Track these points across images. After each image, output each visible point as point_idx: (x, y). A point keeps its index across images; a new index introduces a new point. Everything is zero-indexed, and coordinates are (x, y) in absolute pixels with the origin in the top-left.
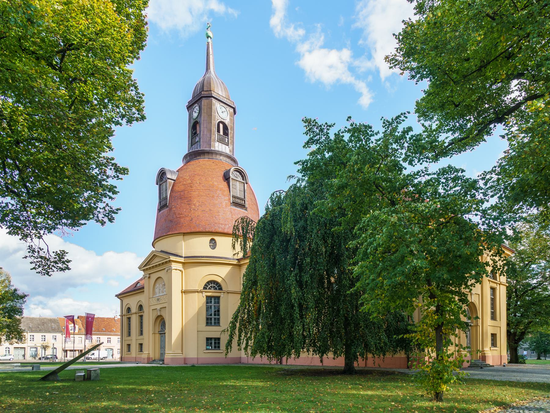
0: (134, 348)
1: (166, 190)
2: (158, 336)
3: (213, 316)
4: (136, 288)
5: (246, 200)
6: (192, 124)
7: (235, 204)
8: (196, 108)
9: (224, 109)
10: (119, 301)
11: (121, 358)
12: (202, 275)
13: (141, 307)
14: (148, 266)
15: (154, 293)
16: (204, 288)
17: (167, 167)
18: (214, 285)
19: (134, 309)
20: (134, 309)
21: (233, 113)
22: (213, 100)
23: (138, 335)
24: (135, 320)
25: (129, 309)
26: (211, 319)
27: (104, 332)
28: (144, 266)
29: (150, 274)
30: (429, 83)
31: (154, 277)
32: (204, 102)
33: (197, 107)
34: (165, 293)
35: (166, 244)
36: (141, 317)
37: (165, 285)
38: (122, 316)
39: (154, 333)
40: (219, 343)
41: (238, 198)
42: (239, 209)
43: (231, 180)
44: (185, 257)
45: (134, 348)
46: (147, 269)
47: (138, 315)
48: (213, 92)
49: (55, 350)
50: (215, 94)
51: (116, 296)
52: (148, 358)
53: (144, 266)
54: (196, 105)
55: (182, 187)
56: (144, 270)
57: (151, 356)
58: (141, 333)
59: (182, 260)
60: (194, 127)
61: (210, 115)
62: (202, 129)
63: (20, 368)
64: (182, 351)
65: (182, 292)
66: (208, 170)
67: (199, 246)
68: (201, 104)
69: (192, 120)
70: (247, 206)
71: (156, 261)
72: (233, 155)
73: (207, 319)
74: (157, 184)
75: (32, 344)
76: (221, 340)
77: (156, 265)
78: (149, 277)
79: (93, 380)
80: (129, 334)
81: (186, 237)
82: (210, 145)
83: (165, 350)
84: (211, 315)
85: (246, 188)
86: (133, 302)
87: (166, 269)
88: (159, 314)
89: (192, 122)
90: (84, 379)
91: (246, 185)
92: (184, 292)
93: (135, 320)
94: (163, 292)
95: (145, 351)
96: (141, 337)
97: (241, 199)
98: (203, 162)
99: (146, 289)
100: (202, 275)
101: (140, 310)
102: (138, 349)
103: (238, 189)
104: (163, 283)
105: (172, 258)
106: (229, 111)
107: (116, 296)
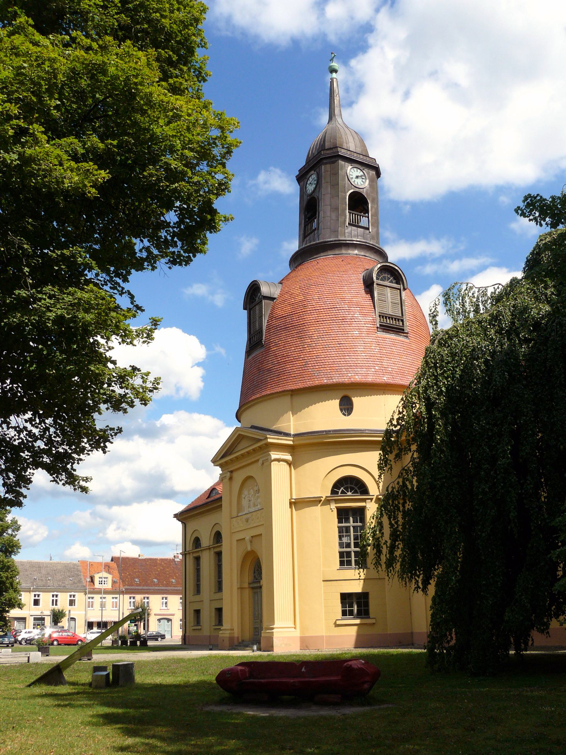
0: (207, 616)
2: (247, 592)
3: (353, 549)
4: (210, 500)
5: (406, 318)
6: (305, 203)
7: (385, 328)
8: (313, 178)
9: (359, 173)
10: (179, 525)
11: (184, 638)
12: (322, 473)
13: (218, 537)
14: (226, 457)
16: (333, 492)
17: (259, 277)
19: (206, 541)
20: (206, 541)
22: (341, 162)
23: (213, 590)
25: (197, 542)
26: (349, 554)
27: (155, 585)
28: (223, 457)
29: (231, 472)
30: (377, 506)
31: (239, 477)
32: (325, 168)
33: (314, 176)
34: (259, 507)
35: (258, 415)
36: (219, 554)
38: (185, 554)
39: (241, 588)
40: (367, 604)
41: (391, 317)
42: (393, 336)
43: (375, 285)
44: (295, 435)
45: (207, 616)
46: (226, 462)
47: (212, 552)
48: (339, 149)
49: (72, 623)
50: (343, 151)
51: (176, 516)
53: (223, 457)
54: (313, 172)
56: (221, 466)
61: (335, 185)
62: (325, 210)
63: (11, 659)
64: (295, 623)
65: (291, 503)
66: (339, 281)
69: (305, 197)
70: (407, 329)
71: (244, 448)
73: (341, 554)
74: (245, 309)
77: (242, 456)
78: (231, 478)
80: (198, 590)
81: (298, 400)
82: (336, 232)
83: (261, 622)
84: (348, 545)
85: (403, 298)
86: (204, 528)
87: (260, 461)
88: (249, 549)
89: (306, 198)
91: (403, 293)
92: (297, 504)
94: (255, 505)
96: (218, 596)
98: (324, 262)
99: (225, 503)
100: (322, 473)
102: (213, 619)
103: (390, 300)
104: (256, 488)
105: (272, 439)
106: (368, 174)
107: (176, 516)
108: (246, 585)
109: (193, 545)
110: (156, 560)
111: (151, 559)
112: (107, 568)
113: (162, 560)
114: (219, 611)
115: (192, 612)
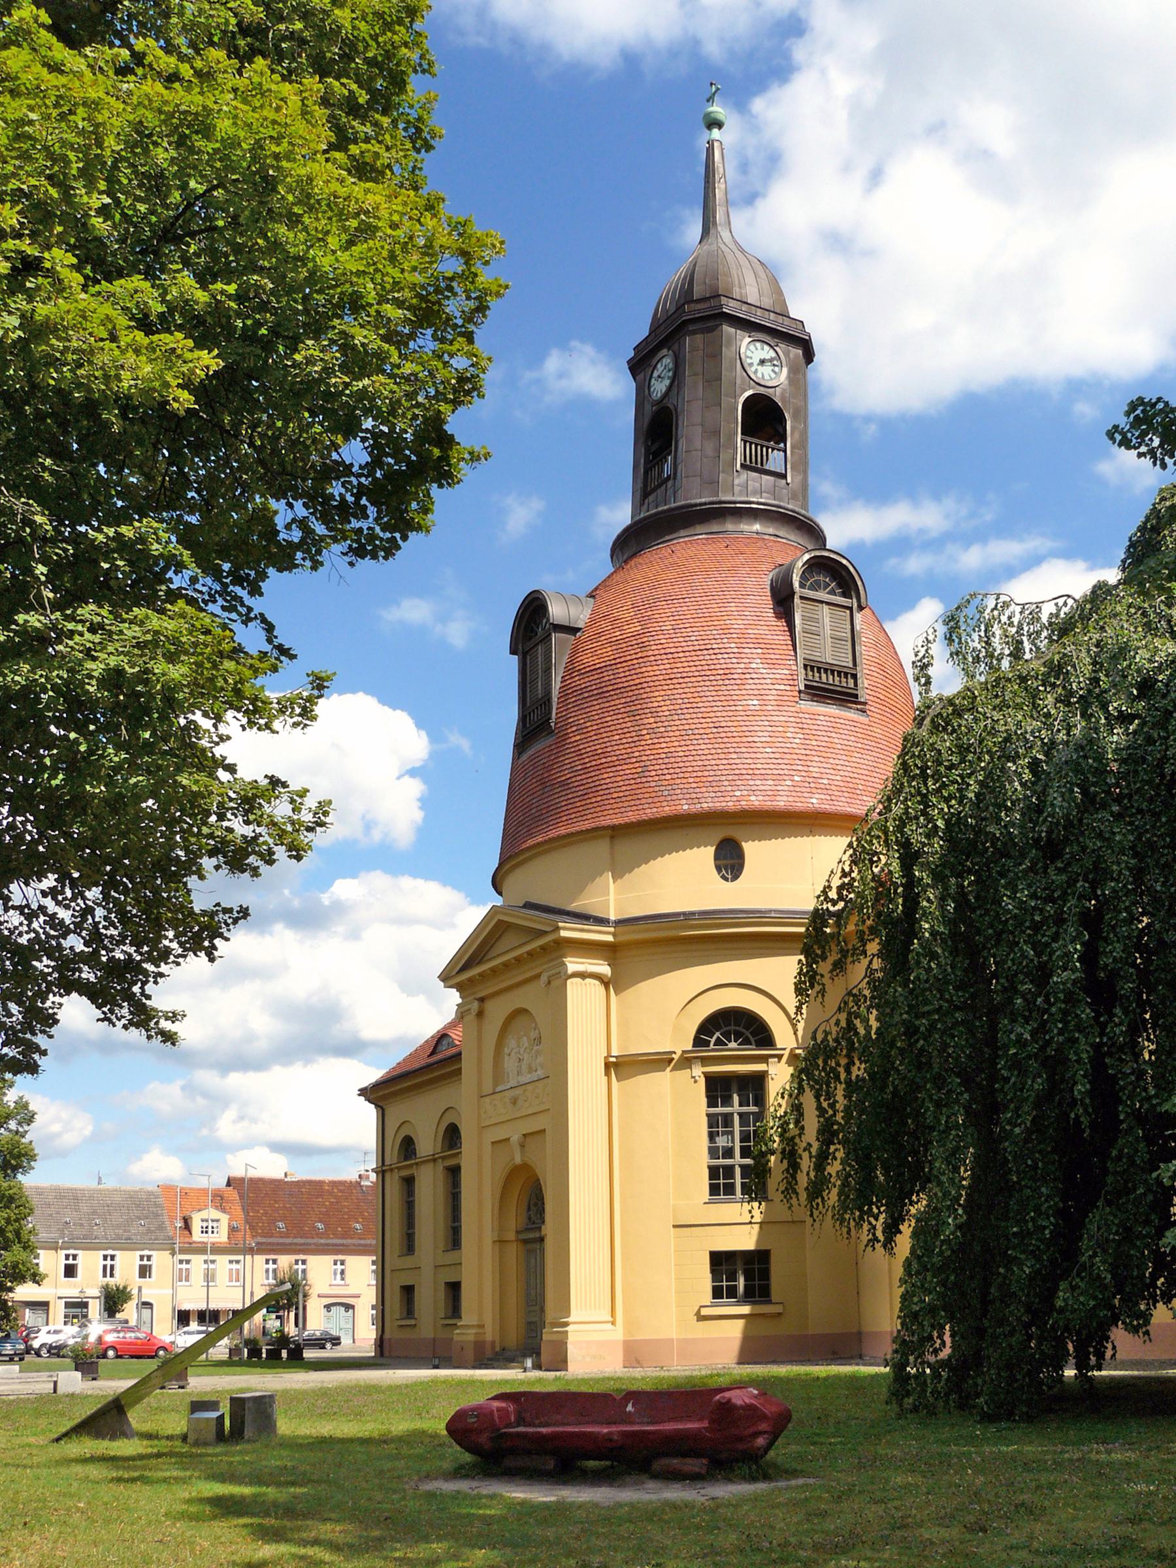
0: (429, 1300)
1: (547, 670)
2: (513, 1250)
3: (738, 1160)
5: (863, 671)
6: (647, 420)
7: (817, 693)
11: (380, 1343)
13: (452, 1135)
14: (471, 970)
15: (498, 1074)
16: (699, 1042)
17: (545, 583)
18: (737, 1026)
19: (427, 1145)
20: (427, 1145)
21: (802, 360)
22: (727, 329)
23: (442, 1246)
24: (429, 1184)
25: (408, 1146)
26: (729, 1171)
27: (320, 1235)
28: (464, 968)
29: (482, 1000)
31: (498, 1010)
33: (668, 361)
34: (540, 1073)
35: (540, 881)
36: (454, 1172)
37: (538, 1040)
38: (382, 1171)
39: (501, 1242)
40: (765, 1274)
41: (830, 670)
42: (833, 710)
43: (797, 600)
44: (619, 923)
45: (429, 1300)
46: (470, 980)
47: (440, 1166)
48: (724, 300)
49: (146, 1312)
50: (732, 303)
51: (363, 1092)
52: (479, 1345)
53: (464, 968)
54: (665, 351)
55: (607, 653)
56: (460, 987)
57: (489, 1334)
58: (454, 1239)
59: (605, 936)
60: (657, 433)
61: (714, 380)
65: (608, 1066)
66: (720, 588)
67: (681, 881)
68: (682, 346)
70: (863, 696)
71: (509, 949)
72: (805, 506)
73: (714, 1172)
74: (513, 652)
75: (71, 1289)
76: (774, 1259)
77: (505, 966)
78: (480, 1014)
79: (249, 1441)
80: (409, 1245)
81: (626, 847)
83: (542, 1310)
84: (729, 1153)
85: (858, 627)
86: (423, 1118)
87: (544, 978)
88: (518, 1160)
89: (649, 410)
90: (220, 1437)
91: (858, 617)
92: (620, 1067)
93: (429, 1184)
94: (531, 1070)
95: (469, 1316)
96: (451, 1257)
97: (842, 673)
98: (688, 550)
101: (451, 1147)
102: (442, 1304)
105: (569, 931)
107: (363, 1092)
108: (511, 1236)
109: (398, 1152)
110: (320, 1183)
111: (310, 1182)
112: (219, 1200)
113: (334, 1184)
114: (454, 1288)
115: (398, 1290)
